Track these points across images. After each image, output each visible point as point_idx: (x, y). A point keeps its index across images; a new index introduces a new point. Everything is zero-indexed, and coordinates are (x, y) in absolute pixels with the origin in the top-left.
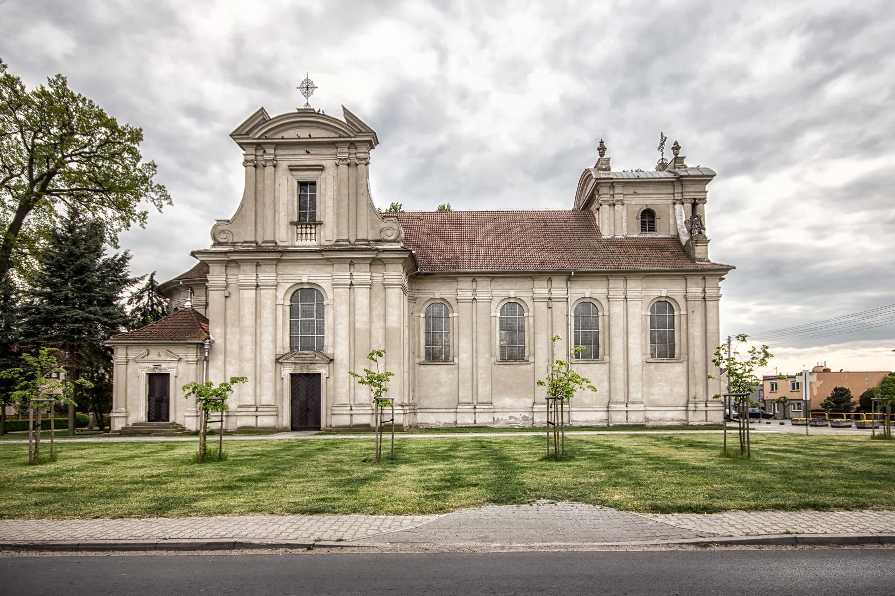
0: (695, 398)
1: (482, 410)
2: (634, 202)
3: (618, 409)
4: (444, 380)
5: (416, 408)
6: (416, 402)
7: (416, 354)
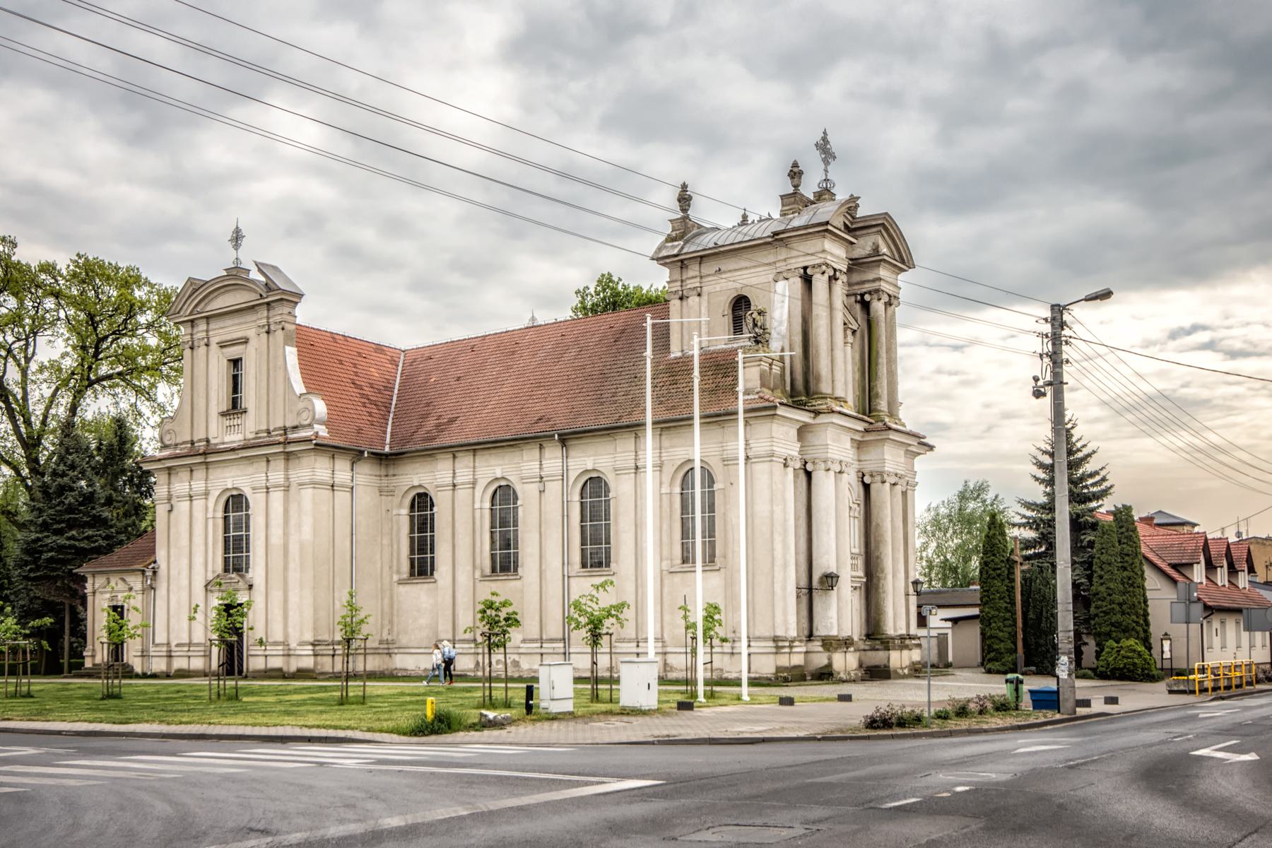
0: (734, 632)
1: (551, 651)
2: (718, 288)
3: (624, 651)
4: (424, 605)
5: (391, 646)
6: (395, 638)
7: (395, 568)
